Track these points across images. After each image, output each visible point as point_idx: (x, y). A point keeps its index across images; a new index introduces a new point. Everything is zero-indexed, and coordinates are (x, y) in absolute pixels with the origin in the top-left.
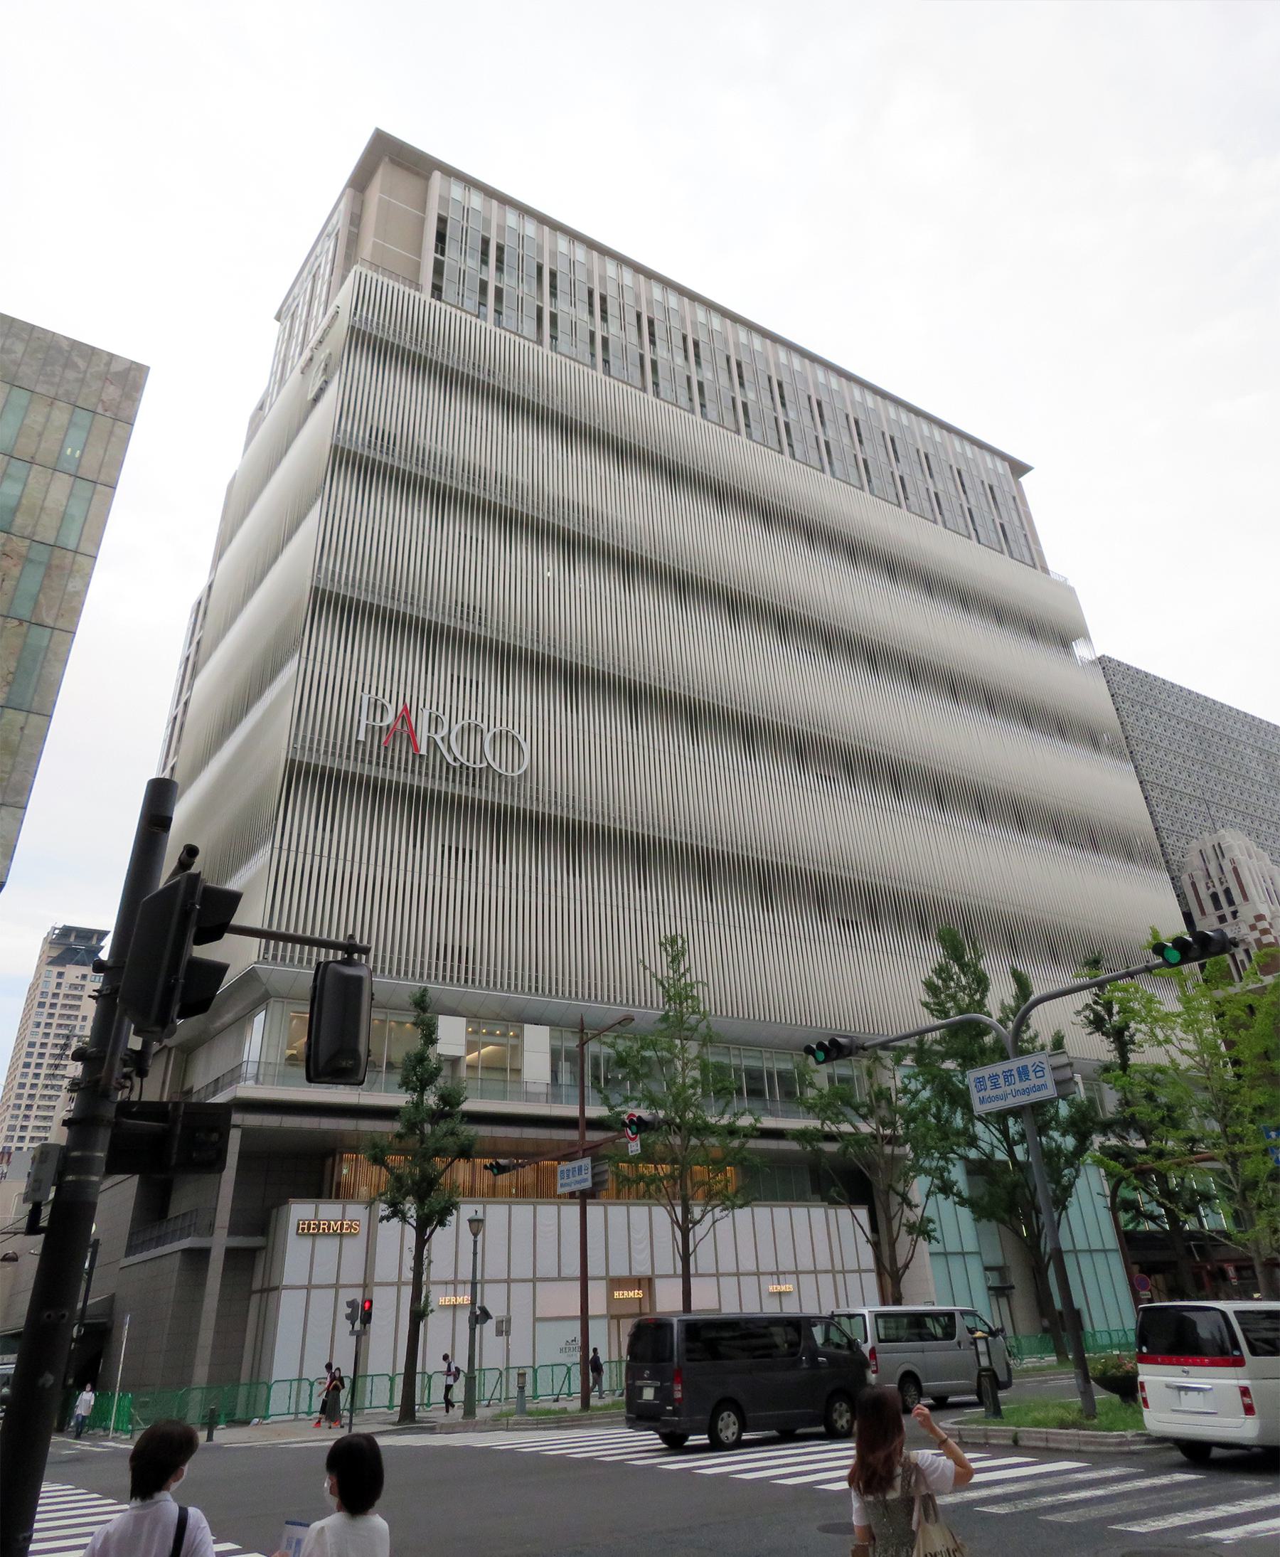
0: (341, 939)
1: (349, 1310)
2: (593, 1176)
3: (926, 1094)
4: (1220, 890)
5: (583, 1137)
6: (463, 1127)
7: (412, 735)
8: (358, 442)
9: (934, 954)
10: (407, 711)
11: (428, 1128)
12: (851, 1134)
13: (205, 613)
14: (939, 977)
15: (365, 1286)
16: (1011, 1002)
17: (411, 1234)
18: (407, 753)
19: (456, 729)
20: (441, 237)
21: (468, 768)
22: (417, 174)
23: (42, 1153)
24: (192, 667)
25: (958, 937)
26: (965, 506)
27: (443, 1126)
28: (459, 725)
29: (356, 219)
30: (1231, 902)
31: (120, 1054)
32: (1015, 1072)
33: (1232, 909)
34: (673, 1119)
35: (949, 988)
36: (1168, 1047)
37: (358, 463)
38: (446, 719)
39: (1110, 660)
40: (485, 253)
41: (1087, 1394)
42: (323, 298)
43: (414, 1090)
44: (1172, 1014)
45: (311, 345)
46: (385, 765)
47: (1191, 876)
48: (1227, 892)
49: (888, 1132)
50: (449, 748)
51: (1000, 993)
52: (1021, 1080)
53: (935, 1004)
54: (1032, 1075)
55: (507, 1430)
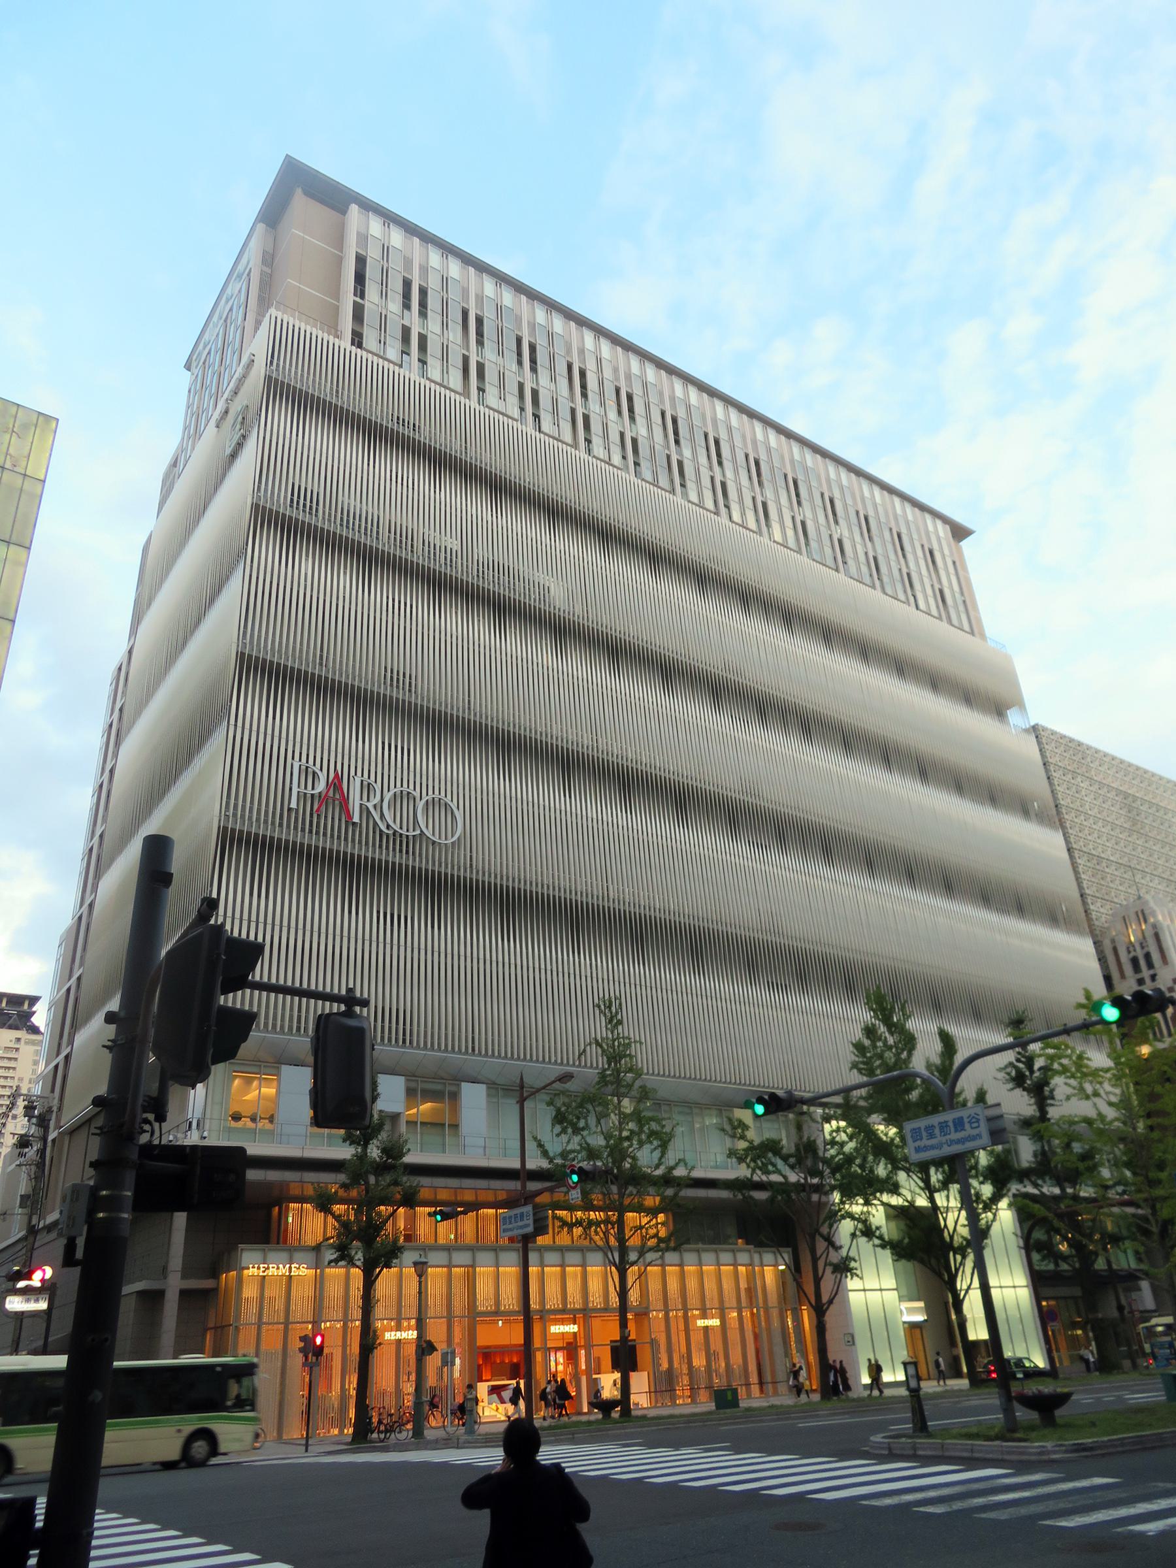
0: (344, 992)
1: (302, 1344)
2: (535, 1221)
3: (850, 1147)
4: (1140, 954)
5: (524, 1186)
6: (405, 1179)
7: (345, 802)
8: (280, 502)
9: (863, 1015)
10: (338, 778)
11: (372, 1179)
12: (781, 1183)
13: (126, 680)
14: (868, 1038)
15: (314, 1323)
16: (937, 1060)
17: (357, 1273)
18: (340, 820)
19: (388, 796)
20: (360, 279)
21: (401, 835)
22: (333, 208)
23: (73, 1192)
24: (115, 735)
25: (887, 998)
26: (905, 571)
27: (388, 1178)
28: (392, 793)
29: (269, 259)
30: (1150, 965)
31: (140, 1101)
32: (951, 1124)
33: (1152, 972)
34: (612, 1169)
35: (875, 1047)
36: (1096, 1100)
37: (283, 523)
38: (378, 787)
39: (1045, 729)
40: (407, 296)
41: (1008, 1411)
42: (237, 345)
43: (359, 1144)
44: (1102, 1070)
45: (225, 396)
46: (317, 833)
47: (1113, 941)
48: (1148, 956)
49: (815, 1181)
50: (382, 816)
51: (926, 1052)
52: (956, 1131)
53: (863, 1063)
54: (967, 1126)
55: (458, 1448)
